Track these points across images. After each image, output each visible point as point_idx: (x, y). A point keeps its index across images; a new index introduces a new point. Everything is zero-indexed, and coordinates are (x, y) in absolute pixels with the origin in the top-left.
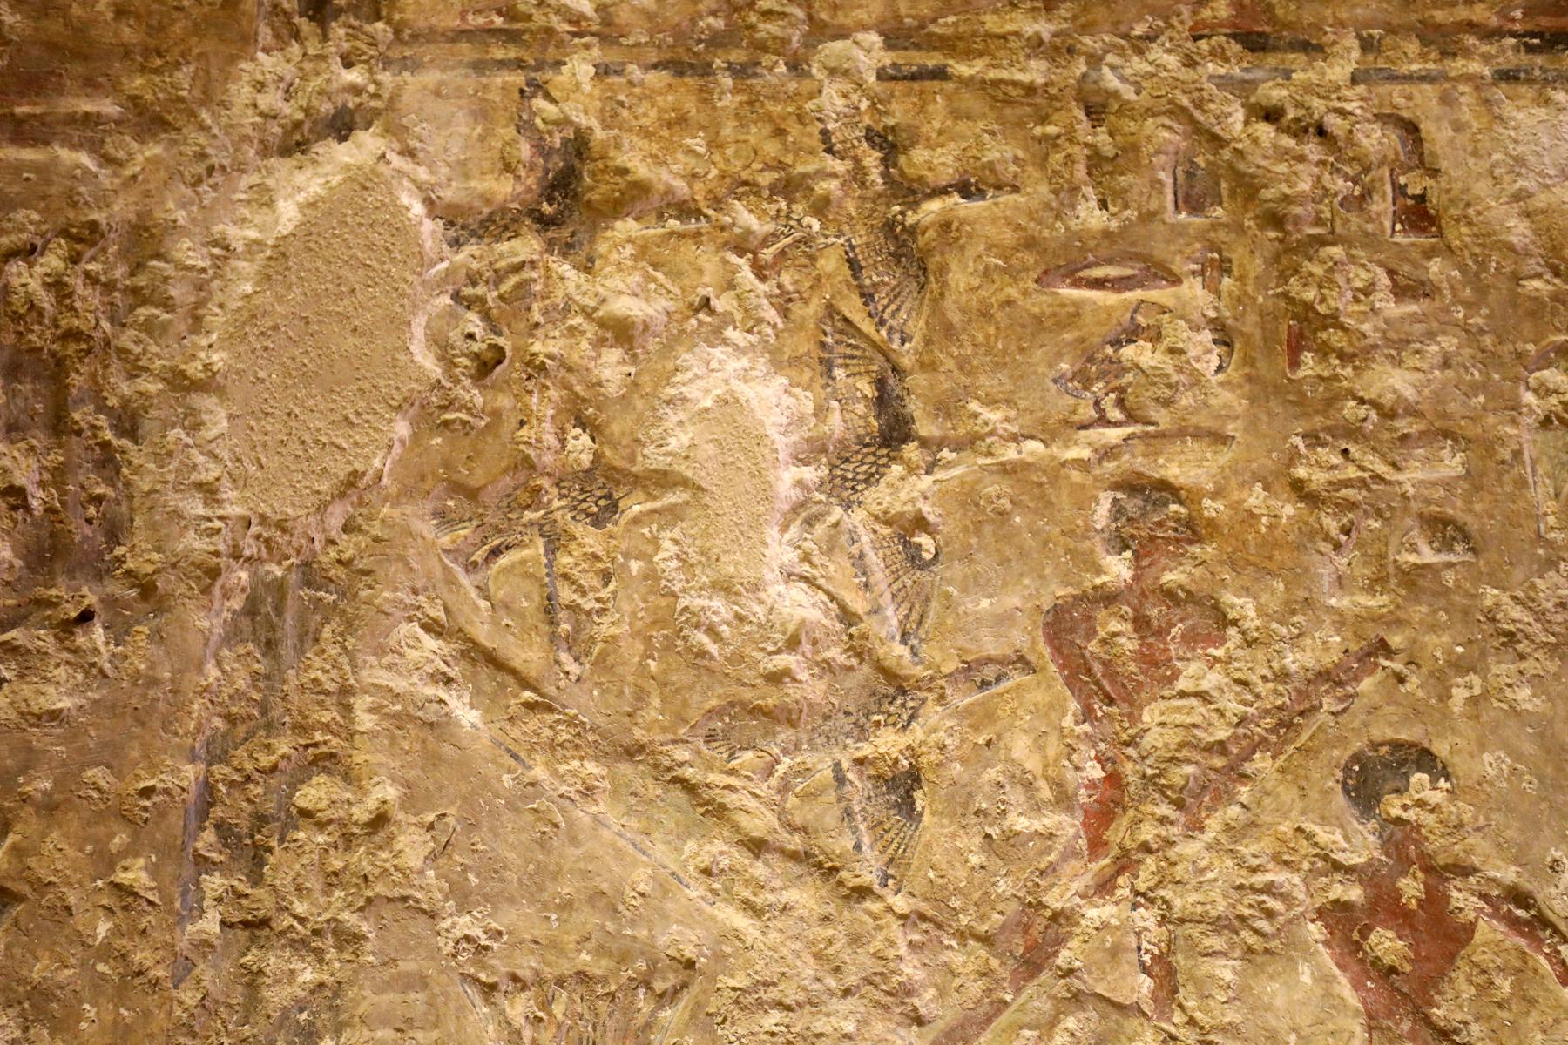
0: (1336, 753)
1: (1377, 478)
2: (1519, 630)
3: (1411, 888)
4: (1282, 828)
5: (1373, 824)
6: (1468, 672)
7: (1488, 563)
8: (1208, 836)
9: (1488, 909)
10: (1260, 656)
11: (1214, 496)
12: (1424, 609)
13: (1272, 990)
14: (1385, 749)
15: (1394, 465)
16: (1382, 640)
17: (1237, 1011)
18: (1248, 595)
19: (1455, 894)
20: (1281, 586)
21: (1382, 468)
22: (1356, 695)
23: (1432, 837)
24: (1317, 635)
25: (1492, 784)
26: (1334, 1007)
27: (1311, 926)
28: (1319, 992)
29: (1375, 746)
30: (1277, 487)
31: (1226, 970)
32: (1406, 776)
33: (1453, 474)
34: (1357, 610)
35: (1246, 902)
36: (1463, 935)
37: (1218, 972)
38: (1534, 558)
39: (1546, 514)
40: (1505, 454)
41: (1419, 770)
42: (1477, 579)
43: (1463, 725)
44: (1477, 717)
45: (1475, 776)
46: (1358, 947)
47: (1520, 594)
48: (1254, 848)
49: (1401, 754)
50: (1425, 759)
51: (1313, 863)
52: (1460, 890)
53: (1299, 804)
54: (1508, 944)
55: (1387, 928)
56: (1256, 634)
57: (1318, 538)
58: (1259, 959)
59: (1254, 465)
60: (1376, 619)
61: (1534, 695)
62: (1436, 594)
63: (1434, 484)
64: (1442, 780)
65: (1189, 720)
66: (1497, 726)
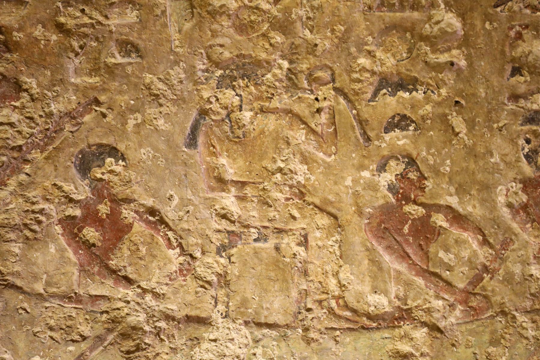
0: (72, 149)
1: (99, 23)
2: (162, 94)
3: (104, 209)
4: (46, 184)
5: (87, 181)
6: (135, 112)
7: (148, 63)
8: (11, 188)
9: (138, 218)
10: (39, 106)
11: (19, 30)
12: (117, 84)
13: (37, 256)
14: (94, 147)
15: (106, 17)
16: (96, 98)
17: (20, 266)
18: (33, 77)
19: (124, 211)
20: (49, 73)
21: (101, 19)
22: (83, 123)
23: (115, 186)
24: (65, 96)
25: (144, 162)
26: (65, 262)
27: (56, 227)
28: (58, 256)
29: (89, 146)
30: (49, 26)
31: (16, 248)
32: (103, 160)
33: (133, 21)
34: (85, 84)
35: (29, 218)
36: (126, 229)
37: (12, 249)
38: (168, 60)
39: (175, 40)
40: (158, 12)
41: (109, 157)
42: (142, 69)
43: (133, 137)
44: (139, 133)
45: (137, 159)
46: (76, 235)
47: (162, 77)
48: (34, 193)
49: (102, 150)
50: (113, 152)
51: (60, 200)
52: (126, 209)
53: (54, 173)
54: (146, 232)
55: (91, 227)
56: (37, 96)
57: (69, 51)
58: (31, 243)
59: (38, 16)
60: (93, 88)
61: (165, 123)
62: (122, 77)
63: (124, 26)
64: (120, 161)
65: (5, 136)
66: (148, 137)
